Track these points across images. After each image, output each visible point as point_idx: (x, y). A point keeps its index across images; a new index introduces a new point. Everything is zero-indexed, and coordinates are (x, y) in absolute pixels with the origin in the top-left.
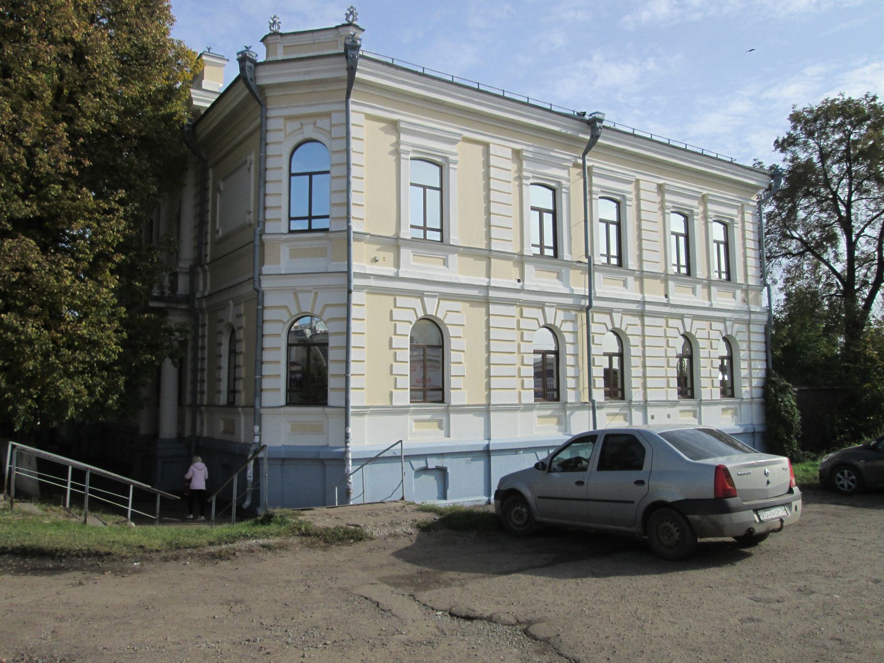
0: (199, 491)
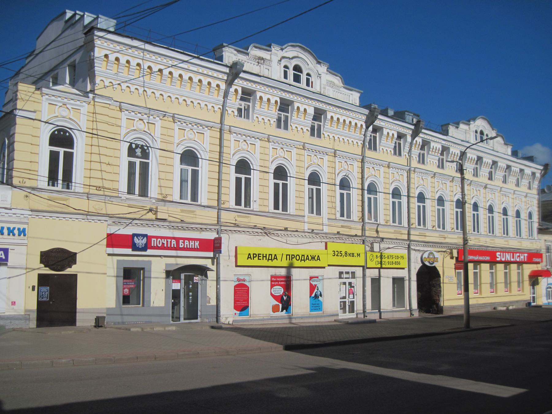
0: (532, 260)
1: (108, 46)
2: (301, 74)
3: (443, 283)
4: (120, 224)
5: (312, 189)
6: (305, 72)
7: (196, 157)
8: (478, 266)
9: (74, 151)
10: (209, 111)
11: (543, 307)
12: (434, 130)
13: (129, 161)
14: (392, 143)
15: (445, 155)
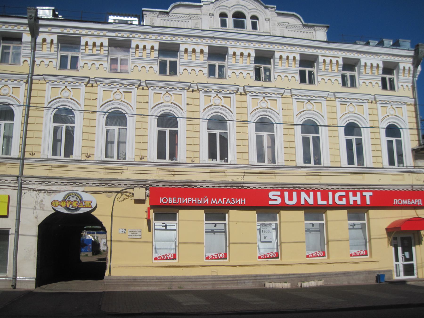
1: (254, 46)
2: (245, 20)
3: (111, 241)
4: (107, 185)
5: (391, 142)
6: (248, 16)
7: (423, 129)
8: (366, 214)
9: (362, 137)
10: (283, 80)
11: (409, 283)
12: (80, 19)
13: (209, 133)
14: (409, 77)
15: (315, 67)
